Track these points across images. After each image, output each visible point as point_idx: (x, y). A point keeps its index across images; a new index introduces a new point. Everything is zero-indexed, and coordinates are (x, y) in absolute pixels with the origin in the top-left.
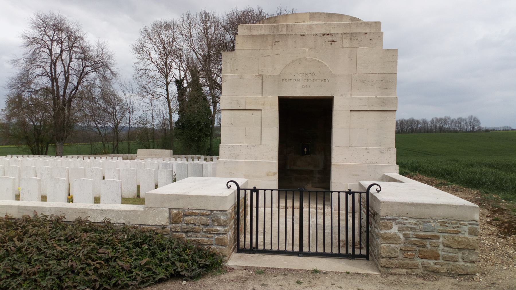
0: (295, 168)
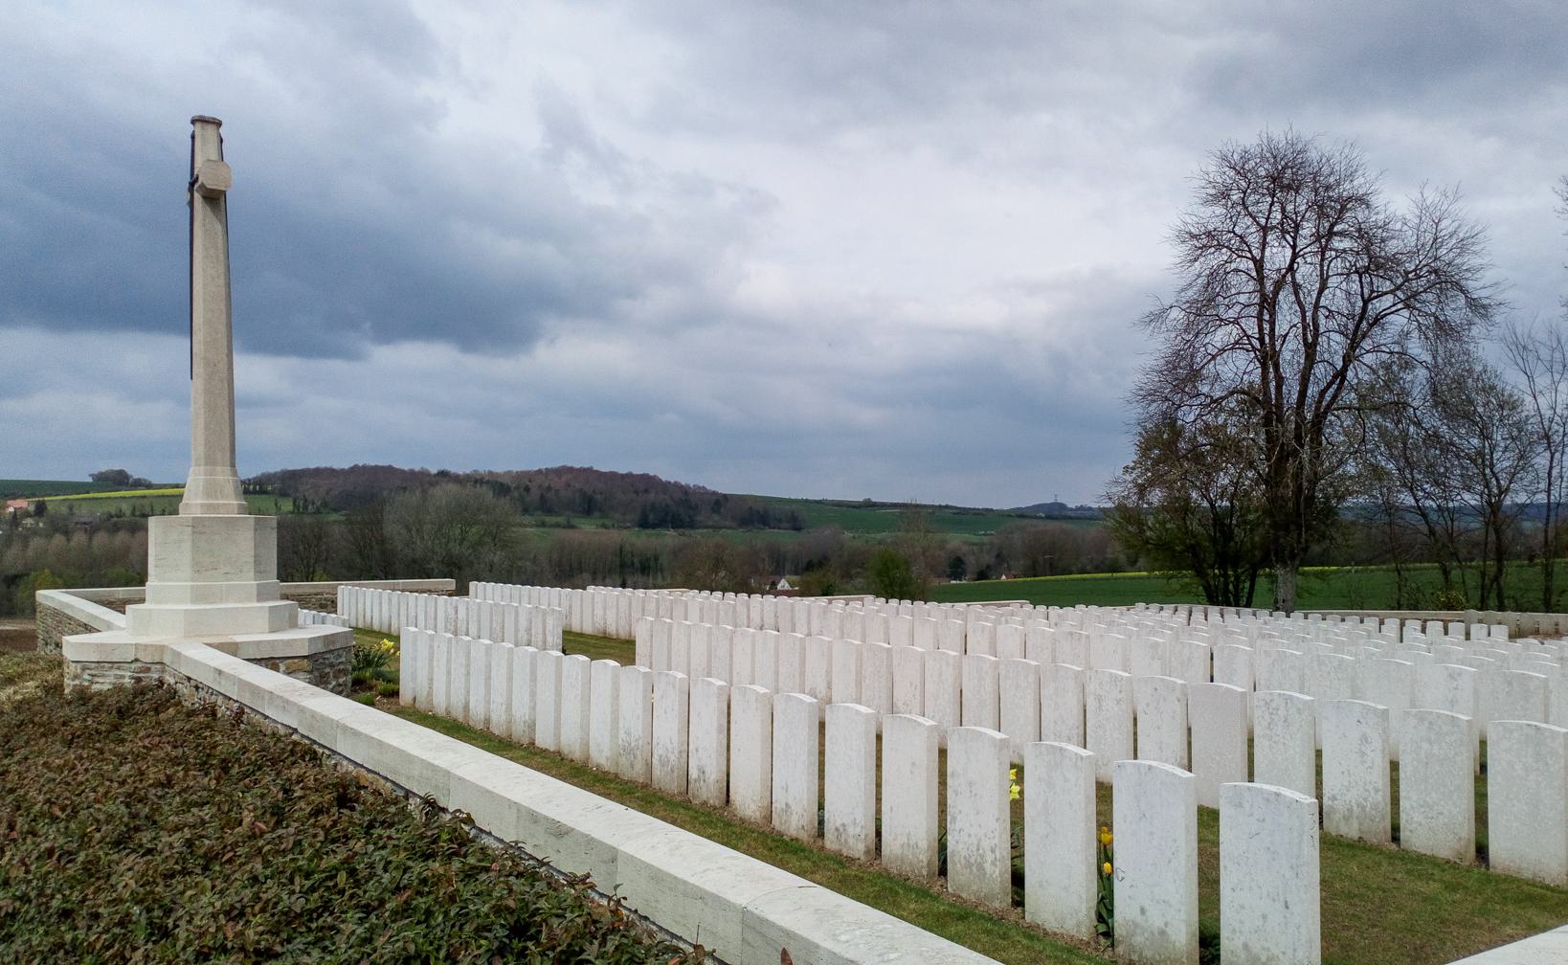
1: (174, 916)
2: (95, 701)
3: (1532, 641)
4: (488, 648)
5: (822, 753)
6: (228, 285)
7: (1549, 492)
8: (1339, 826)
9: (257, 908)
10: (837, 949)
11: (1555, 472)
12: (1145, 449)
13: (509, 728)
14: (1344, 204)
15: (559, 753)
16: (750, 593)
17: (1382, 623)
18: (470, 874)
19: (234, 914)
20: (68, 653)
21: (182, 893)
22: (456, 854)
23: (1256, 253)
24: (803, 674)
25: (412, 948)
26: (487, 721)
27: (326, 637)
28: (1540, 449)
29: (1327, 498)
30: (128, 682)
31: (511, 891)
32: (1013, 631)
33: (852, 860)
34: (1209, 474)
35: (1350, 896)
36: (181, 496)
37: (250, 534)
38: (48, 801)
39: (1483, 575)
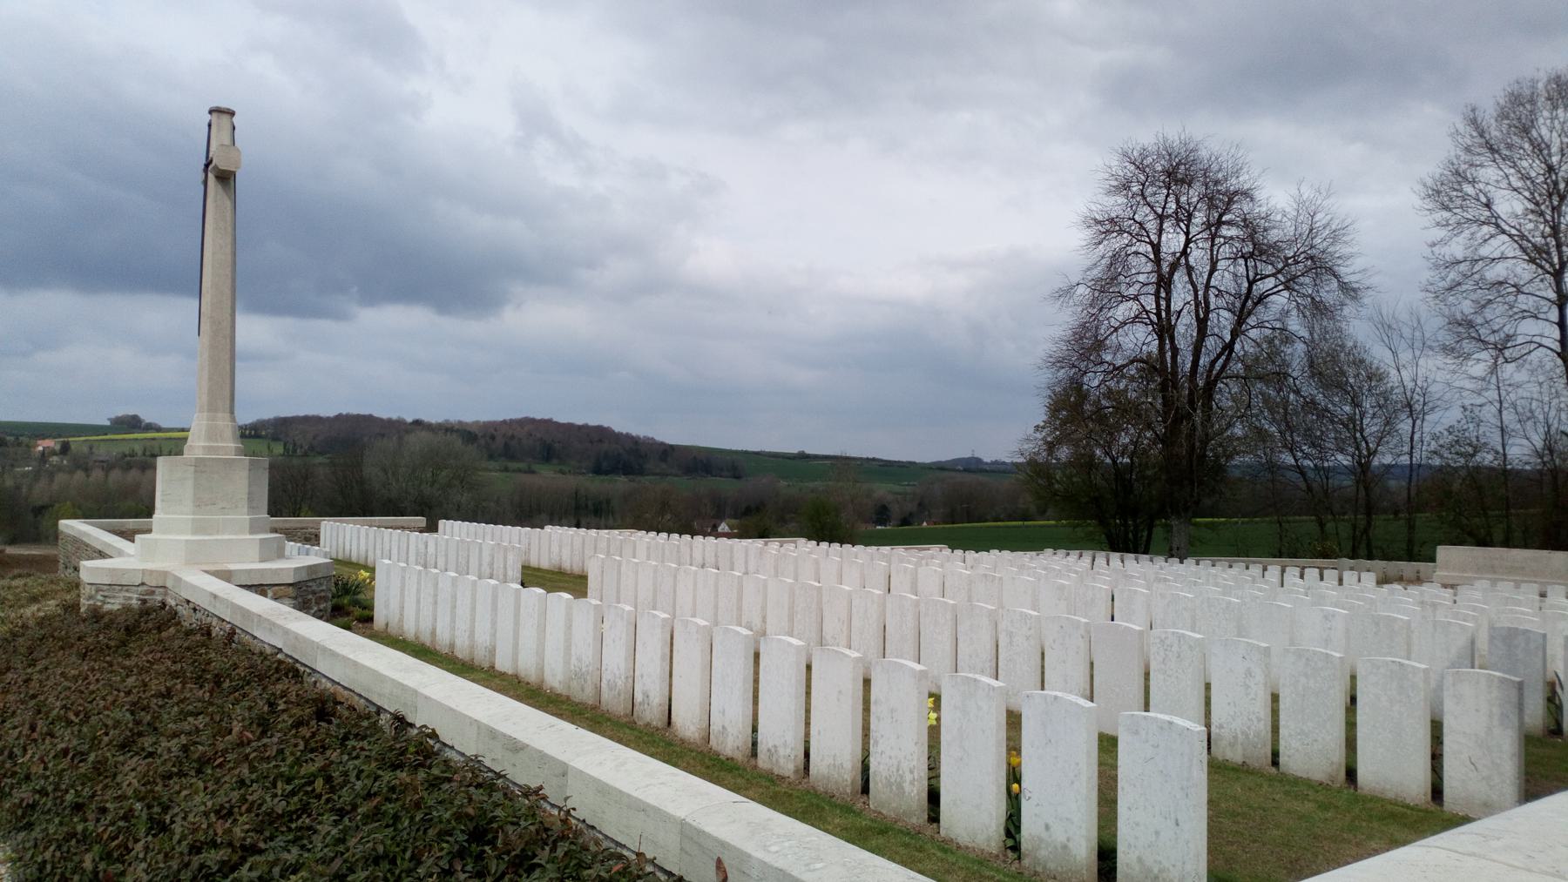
1: (171, 813)
2: (106, 620)
3: (1396, 586)
4: (454, 580)
5: (756, 681)
6: (234, 254)
7: (1411, 454)
8: (1225, 752)
9: (244, 808)
10: (768, 859)
11: (1416, 437)
12: (1055, 409)
13: (471, 653)
14: (1231, 197)
15: (516, 676)
16: (693, 535)
17: (1265, 569)
18: (434, 784)
19: (224, 813)
20: (85, 576)
21: (178, 793)
22: (422, 765)
23: (1154, 238)
24: (740, 608)
25: (381, 849)
26: (452, 646)
27: (310, 567)
28: (1403, 416)
29: (1217, 457)
30: (135, 603)
31: (470, 800)
32: (933, 573)
33: (782, 778)
34: (1111, 434)
35: (1234, 814)
36: (185, 439)
37: (245, 474)
38: (64, 707)
39: (1354, 527)
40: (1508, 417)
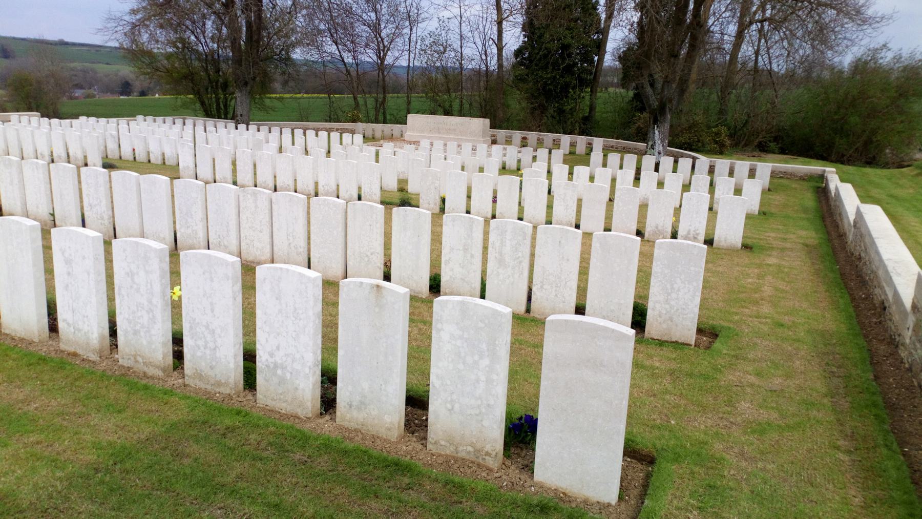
0: (728, 47)
39: (377, 101)
40: (466, 29)
